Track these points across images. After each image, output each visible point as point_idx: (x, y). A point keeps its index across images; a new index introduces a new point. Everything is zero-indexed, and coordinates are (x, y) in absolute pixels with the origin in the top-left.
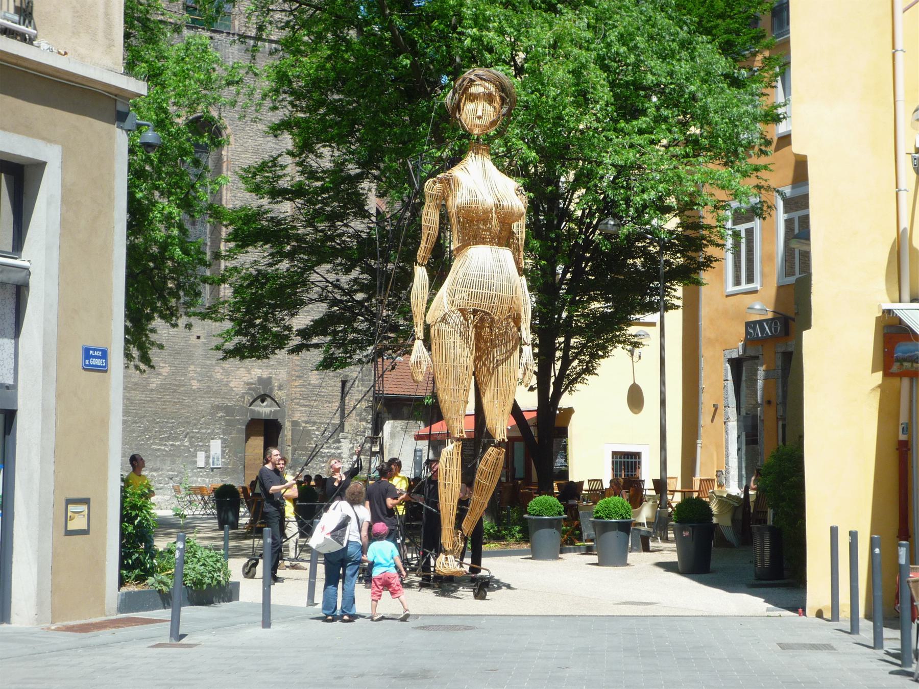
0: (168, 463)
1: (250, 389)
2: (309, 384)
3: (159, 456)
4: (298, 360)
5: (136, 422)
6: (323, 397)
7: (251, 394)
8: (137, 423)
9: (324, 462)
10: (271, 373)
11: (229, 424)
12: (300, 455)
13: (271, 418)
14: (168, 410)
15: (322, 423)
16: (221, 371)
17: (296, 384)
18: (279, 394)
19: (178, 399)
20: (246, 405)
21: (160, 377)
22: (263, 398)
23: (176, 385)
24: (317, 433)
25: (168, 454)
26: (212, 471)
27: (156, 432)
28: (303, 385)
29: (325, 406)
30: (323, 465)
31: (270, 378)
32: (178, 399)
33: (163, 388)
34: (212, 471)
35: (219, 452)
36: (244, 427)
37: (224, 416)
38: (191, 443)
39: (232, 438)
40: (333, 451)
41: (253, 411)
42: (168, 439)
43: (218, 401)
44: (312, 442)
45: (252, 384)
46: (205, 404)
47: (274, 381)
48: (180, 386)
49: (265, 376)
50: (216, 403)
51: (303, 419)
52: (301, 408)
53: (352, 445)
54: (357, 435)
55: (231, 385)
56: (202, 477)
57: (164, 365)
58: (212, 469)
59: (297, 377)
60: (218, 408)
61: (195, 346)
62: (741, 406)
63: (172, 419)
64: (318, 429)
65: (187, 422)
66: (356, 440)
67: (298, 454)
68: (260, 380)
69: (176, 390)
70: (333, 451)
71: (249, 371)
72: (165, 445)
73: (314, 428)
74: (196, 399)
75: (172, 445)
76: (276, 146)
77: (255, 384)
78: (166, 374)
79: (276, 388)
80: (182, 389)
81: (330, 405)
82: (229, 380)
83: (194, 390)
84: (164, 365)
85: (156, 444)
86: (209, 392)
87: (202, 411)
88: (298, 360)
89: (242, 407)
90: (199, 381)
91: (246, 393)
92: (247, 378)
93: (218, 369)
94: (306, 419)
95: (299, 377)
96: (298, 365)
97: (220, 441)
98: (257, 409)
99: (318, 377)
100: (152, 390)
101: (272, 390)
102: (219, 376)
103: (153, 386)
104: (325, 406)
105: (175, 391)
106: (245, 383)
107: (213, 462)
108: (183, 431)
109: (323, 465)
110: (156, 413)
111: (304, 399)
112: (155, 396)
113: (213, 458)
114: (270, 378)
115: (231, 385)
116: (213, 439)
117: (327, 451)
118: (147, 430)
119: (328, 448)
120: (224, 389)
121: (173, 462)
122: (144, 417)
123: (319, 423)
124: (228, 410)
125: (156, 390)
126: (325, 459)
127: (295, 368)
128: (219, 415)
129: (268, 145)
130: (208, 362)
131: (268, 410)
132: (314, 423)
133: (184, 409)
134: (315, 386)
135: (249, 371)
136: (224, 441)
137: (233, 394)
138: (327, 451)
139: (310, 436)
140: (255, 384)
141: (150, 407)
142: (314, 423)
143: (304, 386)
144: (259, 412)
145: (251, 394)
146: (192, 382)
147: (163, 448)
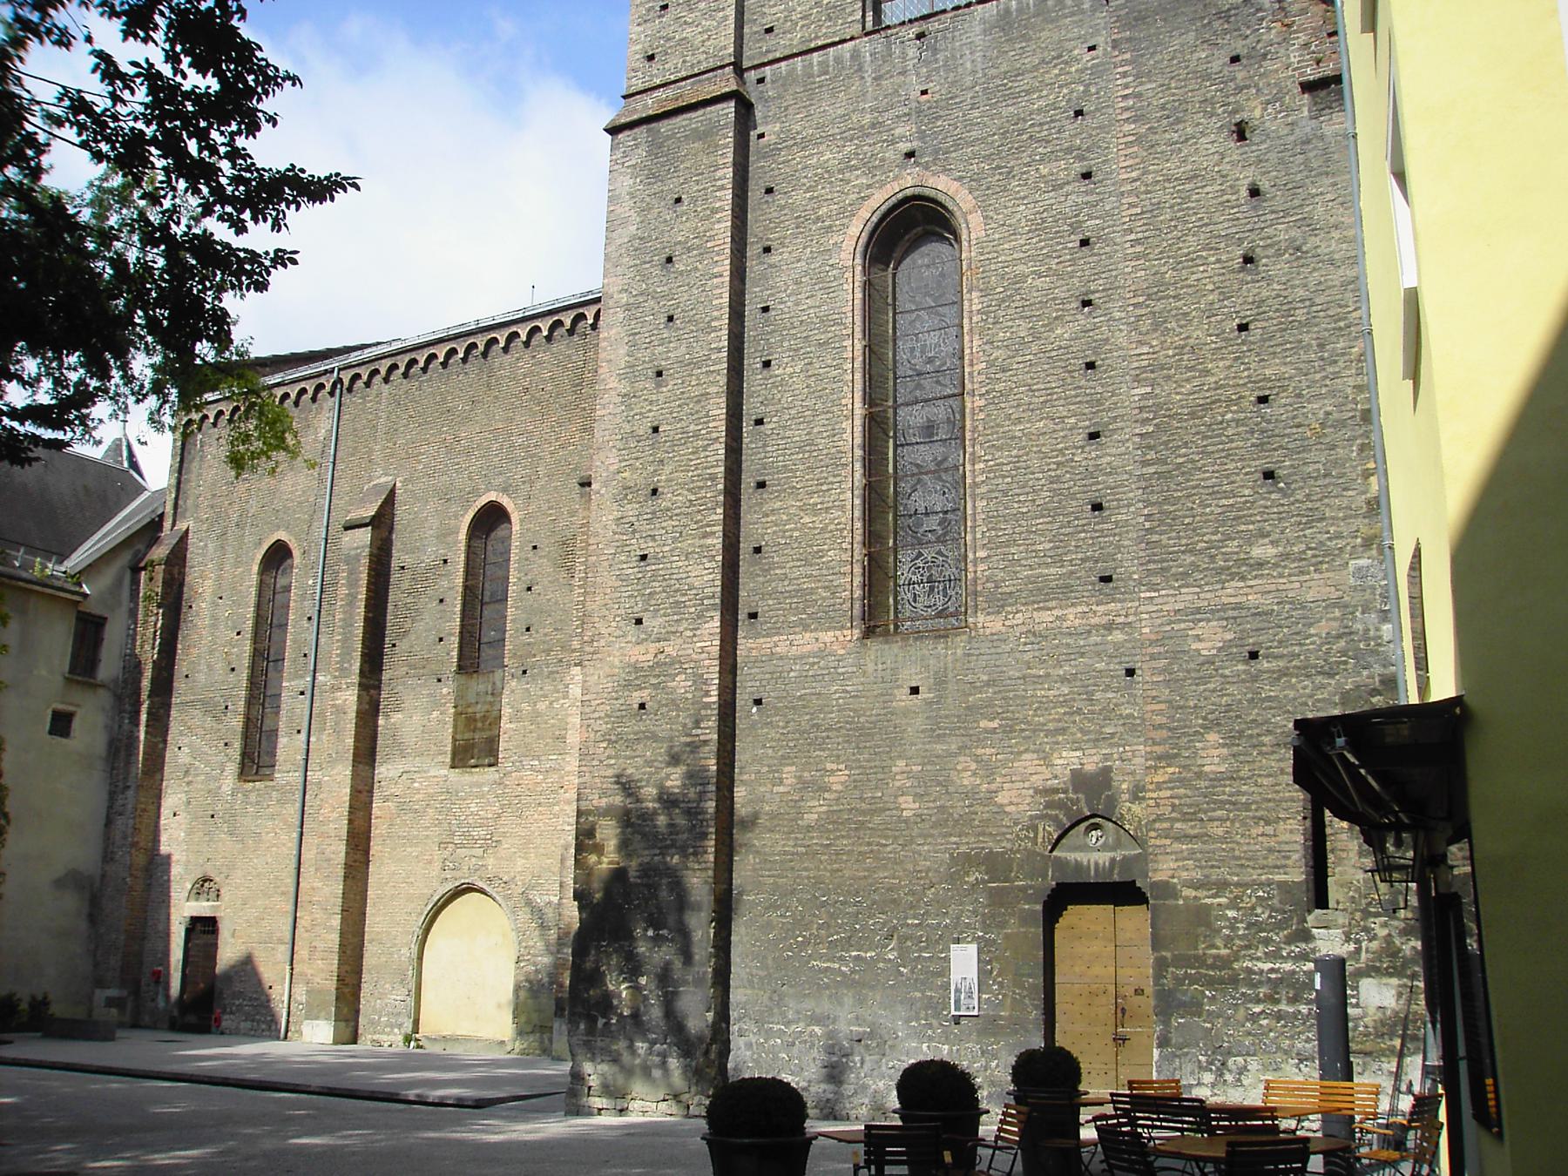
0: (848, 1000)
1: (1048, 805)
2: (1199, 775)
3: (827, 987)
4: (1160, 713)
5: (774, 907)
6: (1247, 807)
7: (1055, 819)
8: (778, 908)
9: (1258, 1001)
10: (1107, 757)
11: (997, 898)
12: (1179, 981)
13: (1116, 878)
14: (847, 873)
15: (1246, 885)
16: (974, 766)
17: (1159, 778)
18: (1132, 811)
19: (869, 844)
20: (1042, 848)
21: (826, 795)
22: (1091, 820)
23: (864, 813)
24: (1231, 914)
25: (848, 982)
26: (957, 1023)
27: (820, 927)
28: (1181, 780)
29: (1254, 832)
30: (1257, 1009)
31: (1107, 771)
32: (869, 844)
33: (832, 821)
34: (957, 1023)
35: (973, 974)
36: (1039, 907)
37: (983, 881)
38: (903, 952)
39: (1007, 936)
40: (1288, 966)
41: (1060, 864)
42: (847, 943)
43: (967, 844)
44: (1219, 942)
45: (1055, 791)
46: (933, 853)
47: (1116, 777)
48: (873, 812)
49: (1090, 768)
50: (963, 849)
51: (1184, 874)
52: (1177, 846)
53: (1352, 947)
54: (1366, 914)
55: (1001, 799)
56: (930, 1039)
57: (834, 767)
58: (957, 1020)
59: (1159, 758)
60: (967, 861)
61: (906, 713)
62: (338, 850)
63: (857, 894)
64: (1233, 905)
65: (894, 901)
66: (1367, 930)
67: (1176, 978)
68: (1080, 780)
69: (863, 823)
70: (1288, 966)
71: (1046, 759)
72: (841, 959)
73: (1223, 900)
74: (912, 842)
75: (858, 958)
76: (1089, 198)
77: (1065, 791)
78: (840, 788)
79: (1125, 797)
80: (877, 820)
81: (1269, 830)
82: (993, 787)
83: (906, 821)
84: (834, 767)
85: (821, 958)
86: (945, 821)
87: (928, 870)
88: (1160, 713)
89: (1031, 854)
90: (918, 797)
91: (1042, 817)
92: (1041, 777)
93: (964, 761)
94: (1198, 875)
95: (1167, 758)
96: (1161, 726)
97: (973, 948)
98: (1072, 856)
99: (1225, 751)
100: (809, 828)
101: (1112, 802)
102: (967, 780)
103: (811, 818)
104: (1254, 832)
105: (861, 826)
106: (1037, 791)
107: (957, 1002)
108: (884, 924)
109: (1257, 1009)
110: (819, 881)
111: (1185, 818)
112: (816, 840)
113: (958, 991)
114: (1107, 771)
115: (1001, 799)
116: (958, 941)
117: (1267, 966)
118: (800, 923)
119: (1269, 957)
120: (983, 812)
121: (861, 1001)
122: (793, 892)
123: (1237, 885)
124: (995, 865)
125: (819, 827)
126: (1263, 991)
127: (1153, 734)
128: (971, 879)
129: (1070, 203)
130: (939, 748)
131: (1103, 858)
132: (1222, 886)
133: (885, 867)
134: (1218, 779)
135: (1046, 759)
136: (984, 947)
137: (1006, 822)
138: (1267, 966)
139: (1208, 925)
140: (1065, 791)
141: (806, 869)
142: (1222, 886)
143: (1183, 782)
144: (1078, 865)
145: (1055, 819)
146: (901, 799)
147: (837, 966)
